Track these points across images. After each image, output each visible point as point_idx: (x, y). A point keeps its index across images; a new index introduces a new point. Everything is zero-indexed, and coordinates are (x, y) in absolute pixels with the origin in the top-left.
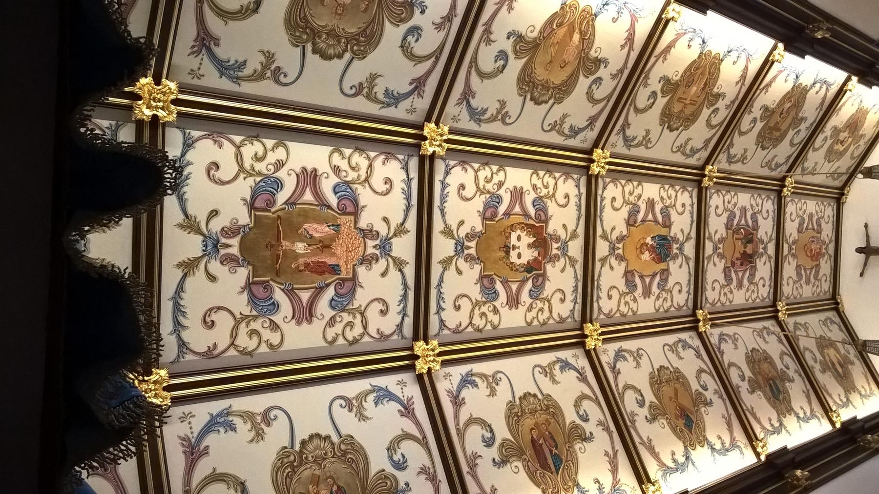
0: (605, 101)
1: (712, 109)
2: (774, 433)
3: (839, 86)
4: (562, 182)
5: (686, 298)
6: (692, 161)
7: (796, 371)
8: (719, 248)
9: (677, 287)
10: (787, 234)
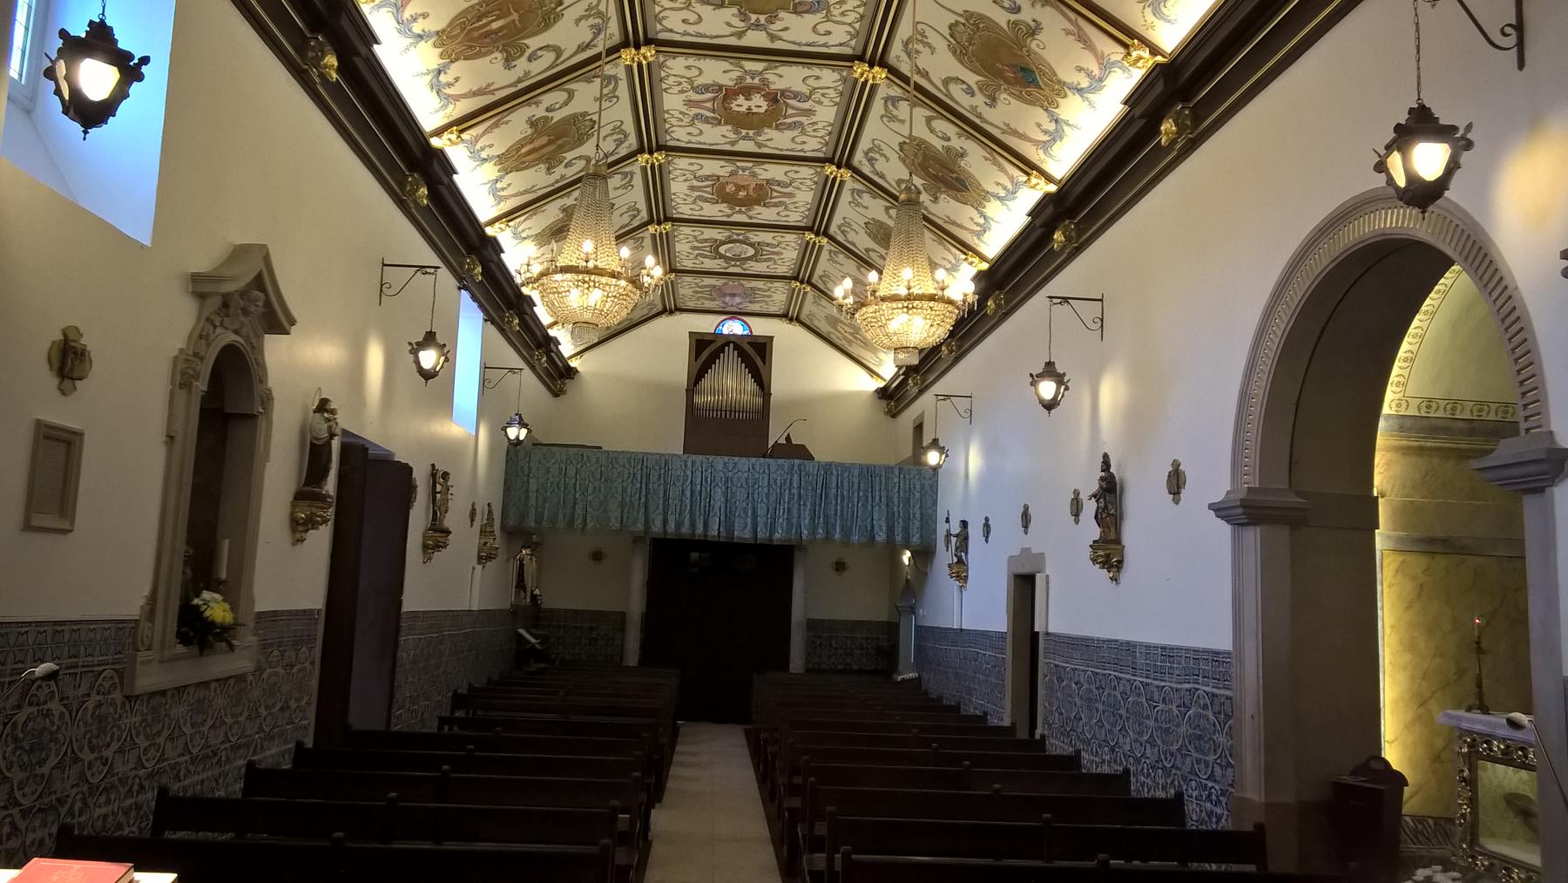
0: (945, 92)
1: (975, 88)
2: (399, 23)
3: (1039, 164)
4: (847, 30)
5: (675, 30)
6: (896, 50)
7: (527, 73)
8: (758, 19)
9: (692, 18)
10: (782, 70)
